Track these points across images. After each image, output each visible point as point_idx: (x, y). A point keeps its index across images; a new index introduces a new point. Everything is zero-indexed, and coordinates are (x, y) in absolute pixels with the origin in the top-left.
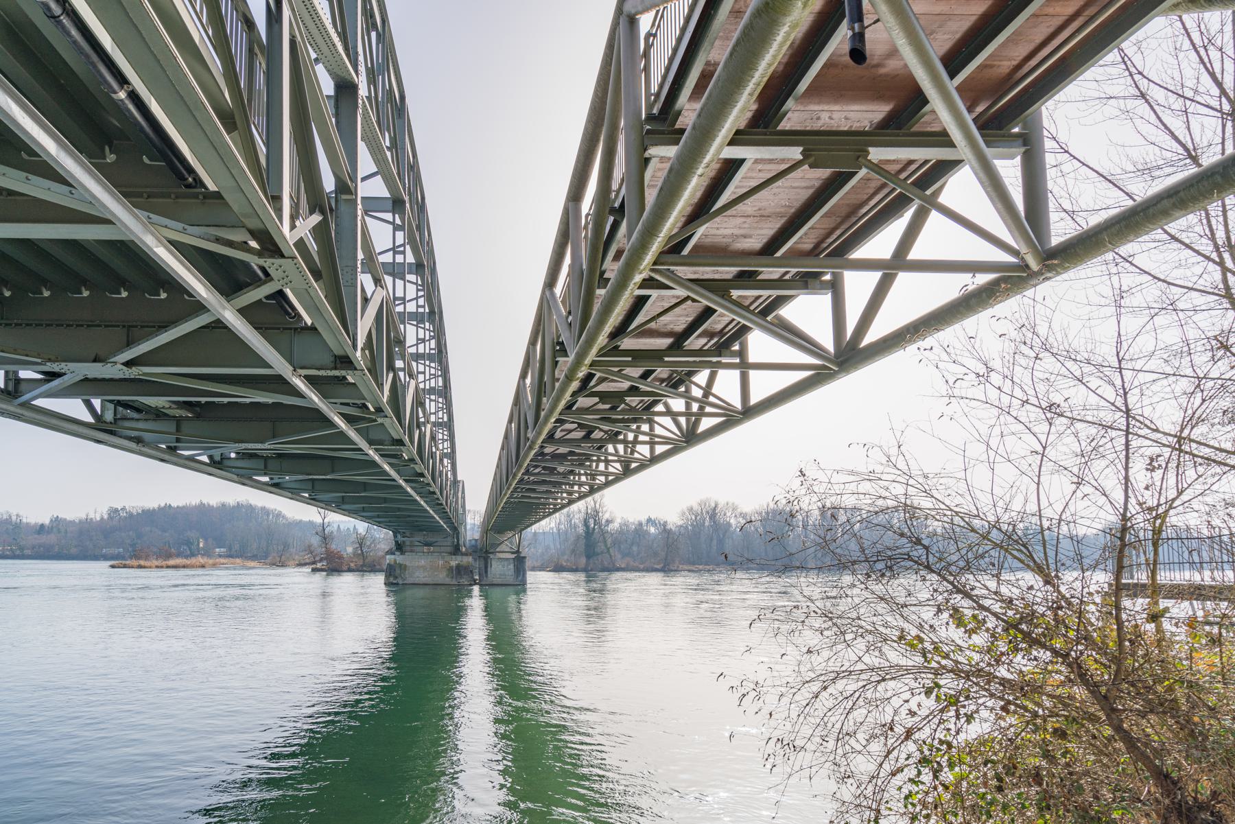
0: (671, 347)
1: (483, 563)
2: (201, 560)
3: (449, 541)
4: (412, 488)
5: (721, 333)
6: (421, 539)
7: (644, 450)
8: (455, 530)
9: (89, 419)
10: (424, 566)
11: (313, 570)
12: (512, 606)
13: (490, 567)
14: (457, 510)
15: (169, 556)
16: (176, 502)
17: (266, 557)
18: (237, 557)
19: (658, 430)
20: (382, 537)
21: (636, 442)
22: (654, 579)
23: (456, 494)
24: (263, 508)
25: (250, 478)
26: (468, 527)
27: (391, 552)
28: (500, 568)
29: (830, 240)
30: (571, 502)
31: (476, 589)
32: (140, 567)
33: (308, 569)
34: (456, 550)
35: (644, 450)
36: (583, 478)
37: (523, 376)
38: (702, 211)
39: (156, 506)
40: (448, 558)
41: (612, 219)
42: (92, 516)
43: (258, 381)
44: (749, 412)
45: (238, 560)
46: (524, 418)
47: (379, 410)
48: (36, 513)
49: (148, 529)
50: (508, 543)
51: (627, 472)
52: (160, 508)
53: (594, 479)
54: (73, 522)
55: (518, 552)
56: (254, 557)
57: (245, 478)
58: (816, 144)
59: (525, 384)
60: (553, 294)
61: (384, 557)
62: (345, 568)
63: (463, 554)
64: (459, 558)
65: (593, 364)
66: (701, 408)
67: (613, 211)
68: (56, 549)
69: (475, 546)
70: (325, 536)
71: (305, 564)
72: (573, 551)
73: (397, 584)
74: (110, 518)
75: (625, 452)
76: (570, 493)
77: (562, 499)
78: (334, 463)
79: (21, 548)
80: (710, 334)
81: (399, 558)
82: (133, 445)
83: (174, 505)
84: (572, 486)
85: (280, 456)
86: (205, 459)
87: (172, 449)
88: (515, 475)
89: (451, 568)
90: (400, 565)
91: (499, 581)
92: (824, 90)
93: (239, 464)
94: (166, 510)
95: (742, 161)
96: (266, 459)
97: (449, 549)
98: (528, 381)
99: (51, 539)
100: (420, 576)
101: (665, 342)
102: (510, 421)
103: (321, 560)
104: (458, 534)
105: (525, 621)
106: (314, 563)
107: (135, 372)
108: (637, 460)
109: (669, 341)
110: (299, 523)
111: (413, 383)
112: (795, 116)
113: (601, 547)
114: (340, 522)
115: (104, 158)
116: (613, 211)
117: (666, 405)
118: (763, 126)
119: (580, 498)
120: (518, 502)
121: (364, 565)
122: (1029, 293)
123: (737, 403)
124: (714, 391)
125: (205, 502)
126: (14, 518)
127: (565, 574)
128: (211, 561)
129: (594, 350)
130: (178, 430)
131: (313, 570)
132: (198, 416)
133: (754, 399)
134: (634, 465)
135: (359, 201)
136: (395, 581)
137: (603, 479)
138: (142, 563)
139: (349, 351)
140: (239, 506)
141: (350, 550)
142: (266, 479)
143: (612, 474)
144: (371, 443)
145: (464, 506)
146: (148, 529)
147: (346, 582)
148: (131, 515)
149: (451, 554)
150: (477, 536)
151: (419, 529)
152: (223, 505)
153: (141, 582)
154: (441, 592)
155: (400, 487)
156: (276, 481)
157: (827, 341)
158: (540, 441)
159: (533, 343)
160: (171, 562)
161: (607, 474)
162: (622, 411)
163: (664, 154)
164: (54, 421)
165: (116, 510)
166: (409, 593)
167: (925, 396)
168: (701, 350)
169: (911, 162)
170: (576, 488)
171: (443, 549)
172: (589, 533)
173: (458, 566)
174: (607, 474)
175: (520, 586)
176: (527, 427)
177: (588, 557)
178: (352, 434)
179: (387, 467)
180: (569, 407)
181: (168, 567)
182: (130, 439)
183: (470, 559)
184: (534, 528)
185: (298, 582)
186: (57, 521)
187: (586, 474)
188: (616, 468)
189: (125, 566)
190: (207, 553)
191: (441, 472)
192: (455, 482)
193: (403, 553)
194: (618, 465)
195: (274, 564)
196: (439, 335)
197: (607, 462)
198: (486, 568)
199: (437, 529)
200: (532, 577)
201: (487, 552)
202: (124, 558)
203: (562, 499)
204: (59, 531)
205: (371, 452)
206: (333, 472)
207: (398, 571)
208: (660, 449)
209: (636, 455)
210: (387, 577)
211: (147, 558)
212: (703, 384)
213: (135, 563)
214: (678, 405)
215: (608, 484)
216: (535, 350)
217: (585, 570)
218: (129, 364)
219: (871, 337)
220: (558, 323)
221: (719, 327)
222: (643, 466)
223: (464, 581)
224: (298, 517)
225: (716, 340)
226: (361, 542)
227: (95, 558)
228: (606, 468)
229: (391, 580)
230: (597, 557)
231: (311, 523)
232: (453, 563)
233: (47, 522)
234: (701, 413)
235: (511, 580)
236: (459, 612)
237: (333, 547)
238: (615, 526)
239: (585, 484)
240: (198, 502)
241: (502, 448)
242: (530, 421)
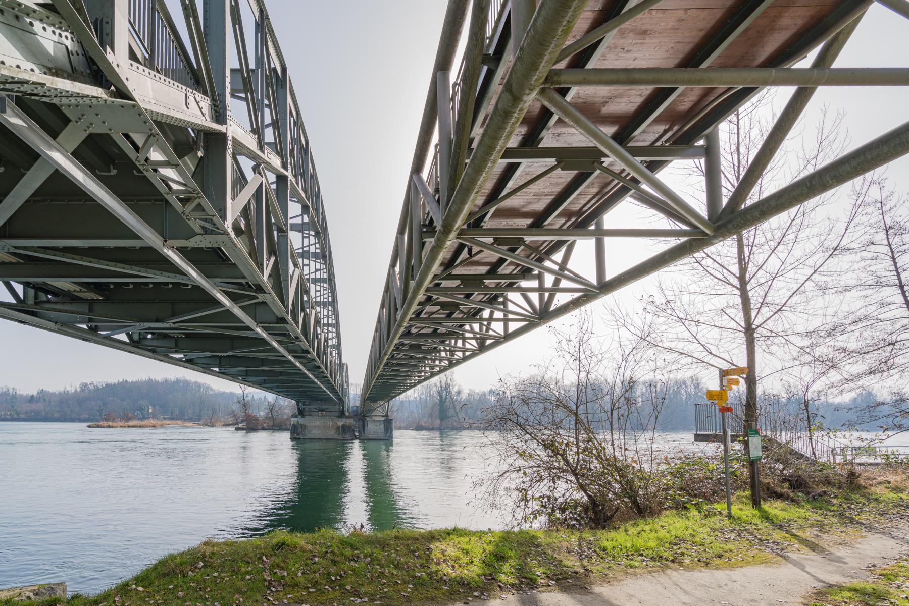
0: (489, 272)
1: (361, 423)
2: (152, 422)
3: (336, 408)
4: (301, 363)
5: (580, 212)
6: (317, 406)
7: (498, 328)
8: (341, 400)
9: (11, 300)
10: (319, 426)
12: (384, 453)
13: (368, 425)
14: (342, 386)
15: (129, 419)
16: (131, 379)
17: (199, 420)
18: (177, 419)
19: (511, 307)
20: (287, 405)
21: (491, 319)
23: (341, 375)
24: (196, 383)
25: (167, 356)
26: (351, 397)
27: (294, 416)
28: (374, 427)
29: (609, 188)
30: (433, 375)
31: (356, 442)
32: (109, 427)
33: (232, 429)
34: (342, 414)
35: (498, 328)
36: (443, 354)
37: (393, 265)
38: (493, 197)
39: (116, 382)
40: (336, 420)
41: (485, 68)
42: (68, 389)
43: (132, 247)
44: (605, 286)
45: (179, 422)
46: (393, 302)
47: (297, 338)
48: (27, 387)
49: (111, 399)
50: (379, 410)
51: (482, 348)
52: (119, 384)
53: (453, 355)
54: (54, 394)
55: (387, 416)
56: (190, 420)
57: (154, 352)
58: (564, 157)
59: (394, 272)
60: (420, 179)
61: (288, 419)
62: (260, 427)
63: (347, 417)
64: (344, 420)
65: (411, 320)
66: (557, 282)
67: (486, 59)
68: (43, 414)
69: (356, 411)
70: (245, 404)
72: (430, 415)
74: (82, 390)
75: (481, 329)
76: (432, 367)
77: (426, 372)
78: (233, 341)
79: (18, 414)
80: (568, 214)
81: (300, 420)
82: (151, 354)
83: (130, 380)
84: (420, 373)
85: (188, 336)
86: (123, 337)
87: (94, 330)
88: (379, 368)
89: (338, 428)
90: (302, 425)
92: (464, 263)
93: (155, 343)
94: (124, 385)
96: (177, 339)
97: (337, 414)
98: (397, 269)
99: (40, 406)
100: (316, 433)
101: (483, 270)
102: (382, 307)
103: (242, 422)
104: (343, 402)
105: (392, 463)
106: (237, 424)
107: (176, 326)
108: (491, 337)
109: (529, 221)
110: (223, 394)
111: (298, 272)
112: (548, 140)
113: (451, 412)
114: (254, 393)
115: (110, 171)
116: (486, 59)
117: (471, 327)
118: (530, 145)
119: (440, 372)
120: (387, 378)
121: (274, 425)
122: (583, 308)
123: (593, 279)
124: (569, 266)
125: (152, 378)
126: (11, 391)
127: (424, 432)
128: (159, 423)
129: (430, 277)
130: (91, 310)
131: (237, 429)
132: (107, 300)
133: (609, 275)
134: (489, 342)
135: (228, 73)
136: (298, 434)
137: (460, 354)
138: (110, 424)
139: (285, 315)
140: (178, 381)
141: (262, 414)
142: (217, 370)
143: (469, 350)
144: (290, 352)
145: (347, 382)
146: (111, 399)
147: (260, 439)
148: (97, 389)
150: (358, 403)
151: (315, 399)
152: (166, 380)
153: (129, 438)
154: (332, 444)
155: (290, 362)
156: (190, 357)
157: (699, 203)
158: (390, 351)
159: (401, 232)
160: (131, 423)
161: (464, 350)
162: (489, 287)
163: (430, 242)
164: (117, 344)
165: (86, 385)
166: (308, 445)
167: (632, 316)
168: (510, 274)
169: (545, 241)
170: (437, 362)
171: (332, 414)
172: (442, 402)
173: (343, 426)
174: (464, 350)
175: (388, 440)
176: (397, 310)
177: (442, 419)
178: (237, 311)
179: (275, 344)
180: (418, 314)
181: (129, 427)
182: (148, 350)
183: (352, 421)
184: (403, 397)
185: (225, 438)
186: (42, 393)
187: (445, 350)
188: (472, 344)
189: (98, 427)
190: (155, 417)
191: (331, 362)
192: (341, 365)
193: (303, 416)
194: (473, 342)
195: (205, 425)
196: (336, 312)
197: (465, 339)
198: (364, 427)
199: (328, 399)
200: (396, 433)
201: (364, 416)
202: (97, 421)
203: (426, 372)
204: (45, 401)
205: (258, 330)
206: (233, 349)
207: (300, 430)
208: (513, 327)
209: (491, 332)
210: (292, 434)
211: (113, 421)
212: (559, 261)
213: (105, 424)
214: (476, 327)
215: (465, 359)
216: (403, 239)
217: (439, 429)
218: (174, 323)
219: (753, 198)
220: (398, 294)
221: (576, 207)
222: (499, 341)
223: (348, 437)
224: (222, 389)
225: (573, 219)
226: (271, 408)
227: (72, 420)
228: (464, 344)
229: (295, 436)
230: (446, 418)
231: (232, 394)
232: (340, 424)
233: (35, 394)
234: (555, 289)
235: (382, 436)
236: (344, 456)
237: (251, 411)
238: (464, 396)
239: (444, 359)
240: (147, 378)
241: (376, 331)
242: (399, 302)
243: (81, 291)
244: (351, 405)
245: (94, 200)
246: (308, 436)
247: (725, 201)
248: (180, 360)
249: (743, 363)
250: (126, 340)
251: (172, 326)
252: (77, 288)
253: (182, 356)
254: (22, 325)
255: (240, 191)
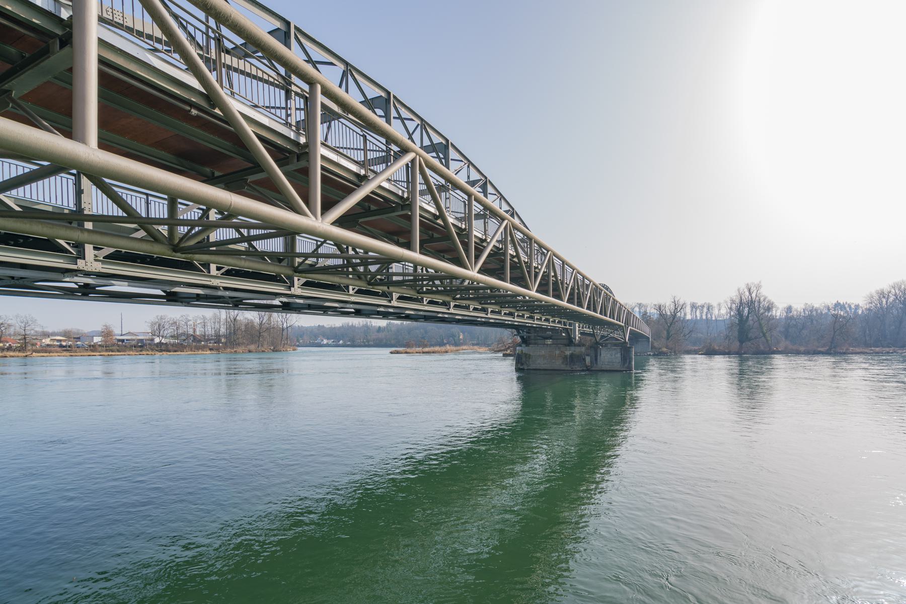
11: (505, 355)
22: (824, 363)
63: (575, 345)
64: (573, 348)
71: (499, 351)
73: (523, 369)
79: (368, 341)
81: (524, 349)
89: (566, 356)
90: (526, 355)
91: (608, 367)
95: (333, 224)
100: (541, 363)
131: (505, 355)
138: (408, 350)
149: (566, 345)
160: (426, 349)
173: (572, 355)
207: (524, 359)
217: (738, 353)
232: (568, 353)
235: (617, 366)
244: (669, 313)
245: (247, 150)
246: (533, 366)
249: (258, 376)
254: (287, 18)
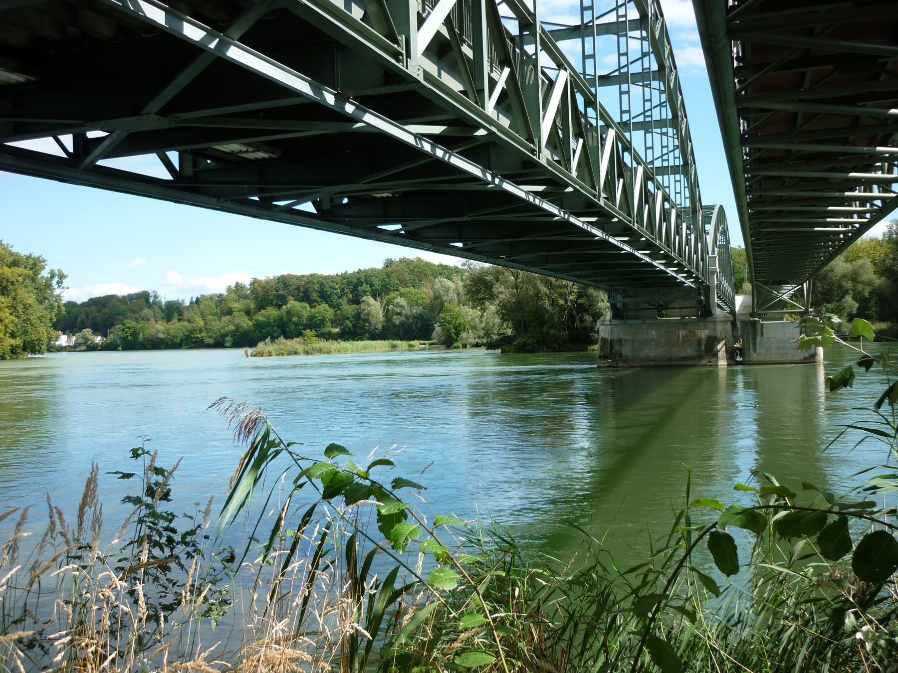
9: (166, 175)
16: (294, 273)
39: (126, 294)
83: (350, 271)
86: (308, 207)
142: (460, 245)
156: (412, 226)
243: (247, 152)
247: (177, 167)
248: (395, 234)
250: (314, 211)
251: (366, 187)
252: (244, 149)
253: (399, 226)
255: (449, 15)
